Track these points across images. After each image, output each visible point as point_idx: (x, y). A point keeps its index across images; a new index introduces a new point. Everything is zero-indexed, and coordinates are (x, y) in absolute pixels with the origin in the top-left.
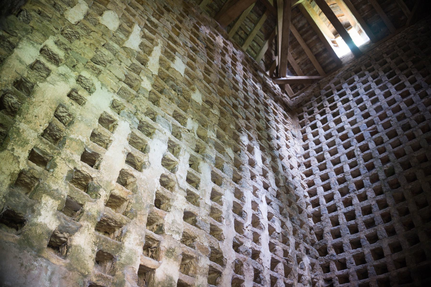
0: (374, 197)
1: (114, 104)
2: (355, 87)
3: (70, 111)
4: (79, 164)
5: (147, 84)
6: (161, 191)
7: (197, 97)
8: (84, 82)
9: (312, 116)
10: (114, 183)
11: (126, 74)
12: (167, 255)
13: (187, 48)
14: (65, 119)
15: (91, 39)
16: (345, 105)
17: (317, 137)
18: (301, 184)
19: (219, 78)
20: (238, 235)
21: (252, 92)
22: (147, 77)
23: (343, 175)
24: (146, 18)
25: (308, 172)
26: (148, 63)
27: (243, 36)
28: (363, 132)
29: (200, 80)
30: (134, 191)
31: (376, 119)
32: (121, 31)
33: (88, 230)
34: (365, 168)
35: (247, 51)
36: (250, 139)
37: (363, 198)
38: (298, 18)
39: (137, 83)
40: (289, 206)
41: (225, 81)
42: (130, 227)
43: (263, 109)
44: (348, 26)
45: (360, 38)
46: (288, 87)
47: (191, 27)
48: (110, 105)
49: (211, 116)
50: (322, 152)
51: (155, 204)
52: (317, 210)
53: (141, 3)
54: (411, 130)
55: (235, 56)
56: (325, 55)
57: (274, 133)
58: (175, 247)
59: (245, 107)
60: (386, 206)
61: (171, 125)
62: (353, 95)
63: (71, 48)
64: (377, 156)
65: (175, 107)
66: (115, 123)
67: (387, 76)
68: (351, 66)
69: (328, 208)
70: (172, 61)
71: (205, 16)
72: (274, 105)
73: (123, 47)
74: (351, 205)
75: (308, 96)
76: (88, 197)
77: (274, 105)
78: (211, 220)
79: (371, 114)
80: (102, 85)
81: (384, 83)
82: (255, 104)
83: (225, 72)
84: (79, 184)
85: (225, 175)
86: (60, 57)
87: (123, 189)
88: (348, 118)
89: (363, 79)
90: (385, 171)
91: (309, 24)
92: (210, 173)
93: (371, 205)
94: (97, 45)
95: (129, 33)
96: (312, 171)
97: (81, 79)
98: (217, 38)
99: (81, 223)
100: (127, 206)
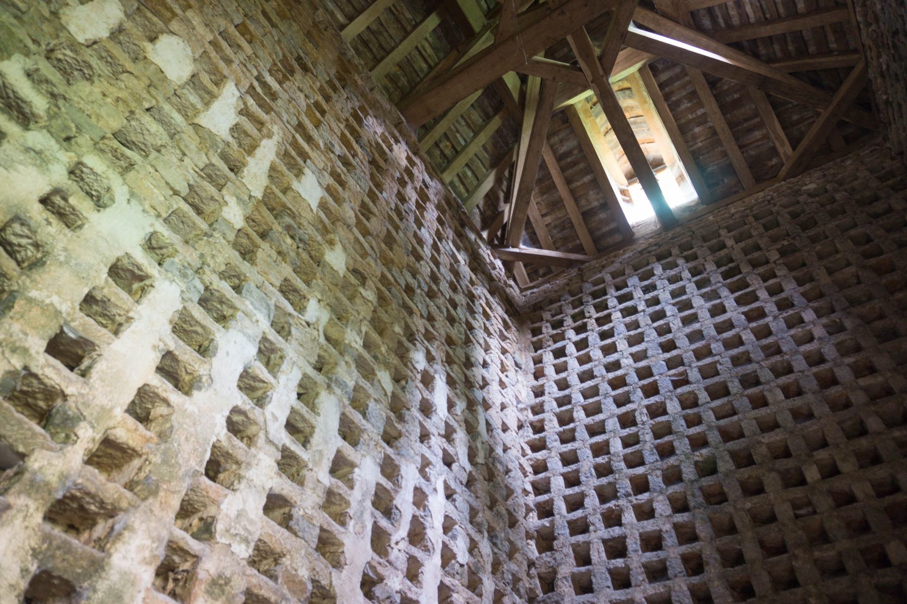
0: (670, 516)
1: (153, 242)
2: (653, 287)
3: (41, 237)
4: (38, 361)
5: (234, 214)
6: (225, 443)
7: (337, 259)
8: (87, 180)
9: (559, 331)
10: (119, 412)
11: (191, 182)
12: (209, 593)
13: (332, 155)
14: (23, 253)
15: (120, 89)
16: (628, 319)
17: (563, 375)
18: (520, 464)
19: (388, 230)
20: (377, 558)
21: (448, 266)
22: (238, 198)
23: (607, 460)
24: (255, 73)
25: (537, 442)
26: (245, 170)
27: (448, 152)
28: (657, 378)
29: (348, 226)
30: (163, 436)
31: (689, 356)
32: (194, 89)
33: (25, 518)
34: (655, 451)
35: (452, 183)
36: (430, 358)
37: (645, 513)
38: (562, 135)
39: (213, 206)
40: (491, 508)
41: (397, 237)
42: (136, 519)
43: (464, 304)
44: (659, 164)
45: (679, 190)
46: (520, 269)
47: (348, 115)
48: (143, 242)
49: (358, 301)
50: (569, 407)
51: (207, 470)
52: (548, 525)
53: (248, 37)
54: (761, 387)
55: (425, 190)
56: (602, 216)
57: (479, 355)
58: (233, 574)
59: (430, 294)
60: (694, 538)
61: (273, 307)
62: (646, 301)
63: (67, 96)
64: (681, 429)
65: (287, 270)
66: (147, 282)
67: (721, 273)
68: (650, 245)
69: (570, 523)
70: (297, 176)
71: (378, 97)
72: (486, 299)
73: (193, 124)
74: (620, 524)
75: (556, 291)
76: (45, 438)
77: (486, 299)
78: (323, 519)
79: (678, 345)
80: (132, 194)
81: (713, 287)
82: (450, 291)
83: (401, 219)
84: (27, 405)
85: (368, 426)
86: (35, 110)
87: (136, 430)
88: (630, 345)
89: (672, 272)
90: (696, 463)
91: (581, 150)
92: (338, 416)
93: (661, 531)
94: (133, 105)
95: (213, 96)
96: (545, 442)
97: (82, 172)
98: (395, 147)
99: (11, 499)
100: (140, 469)
